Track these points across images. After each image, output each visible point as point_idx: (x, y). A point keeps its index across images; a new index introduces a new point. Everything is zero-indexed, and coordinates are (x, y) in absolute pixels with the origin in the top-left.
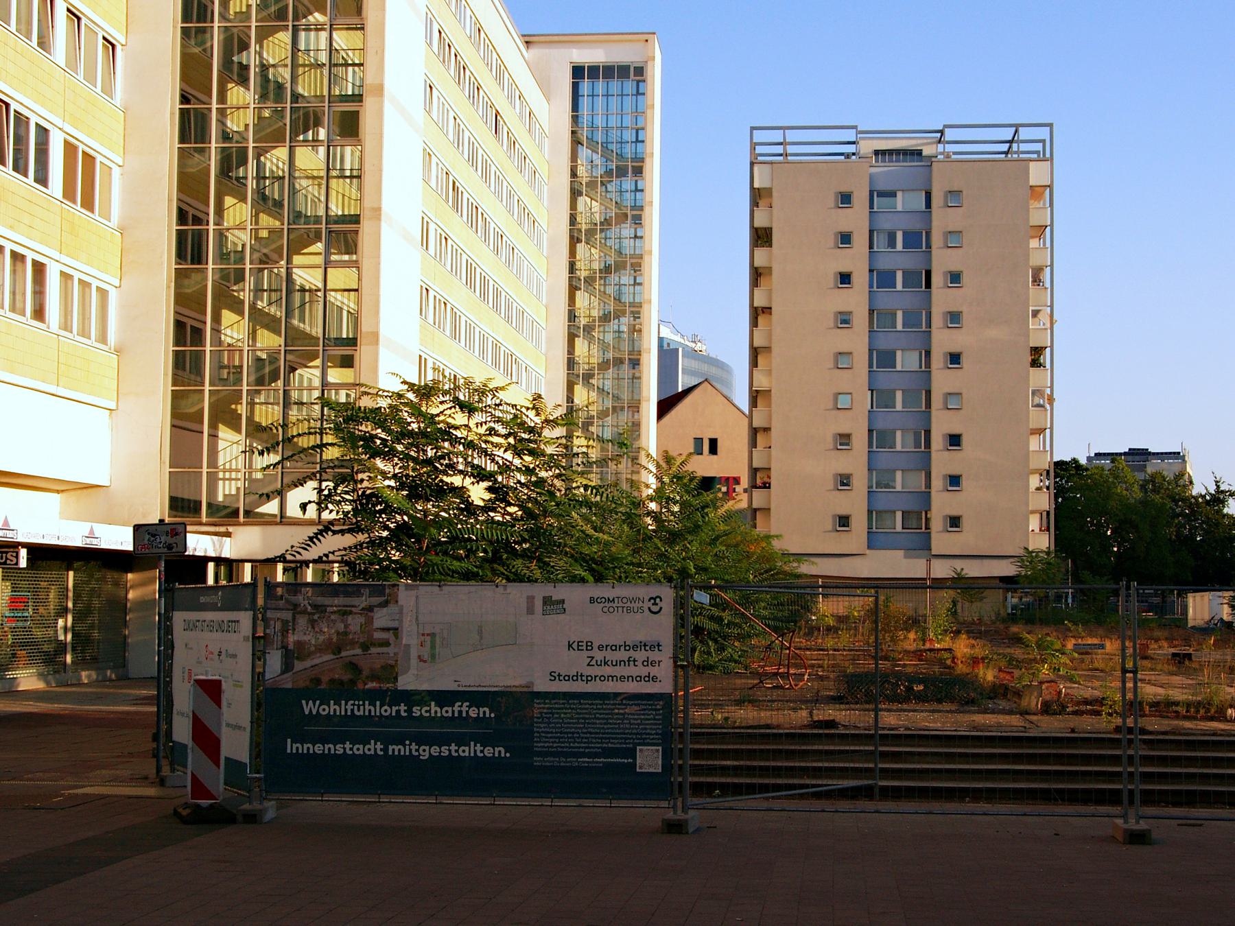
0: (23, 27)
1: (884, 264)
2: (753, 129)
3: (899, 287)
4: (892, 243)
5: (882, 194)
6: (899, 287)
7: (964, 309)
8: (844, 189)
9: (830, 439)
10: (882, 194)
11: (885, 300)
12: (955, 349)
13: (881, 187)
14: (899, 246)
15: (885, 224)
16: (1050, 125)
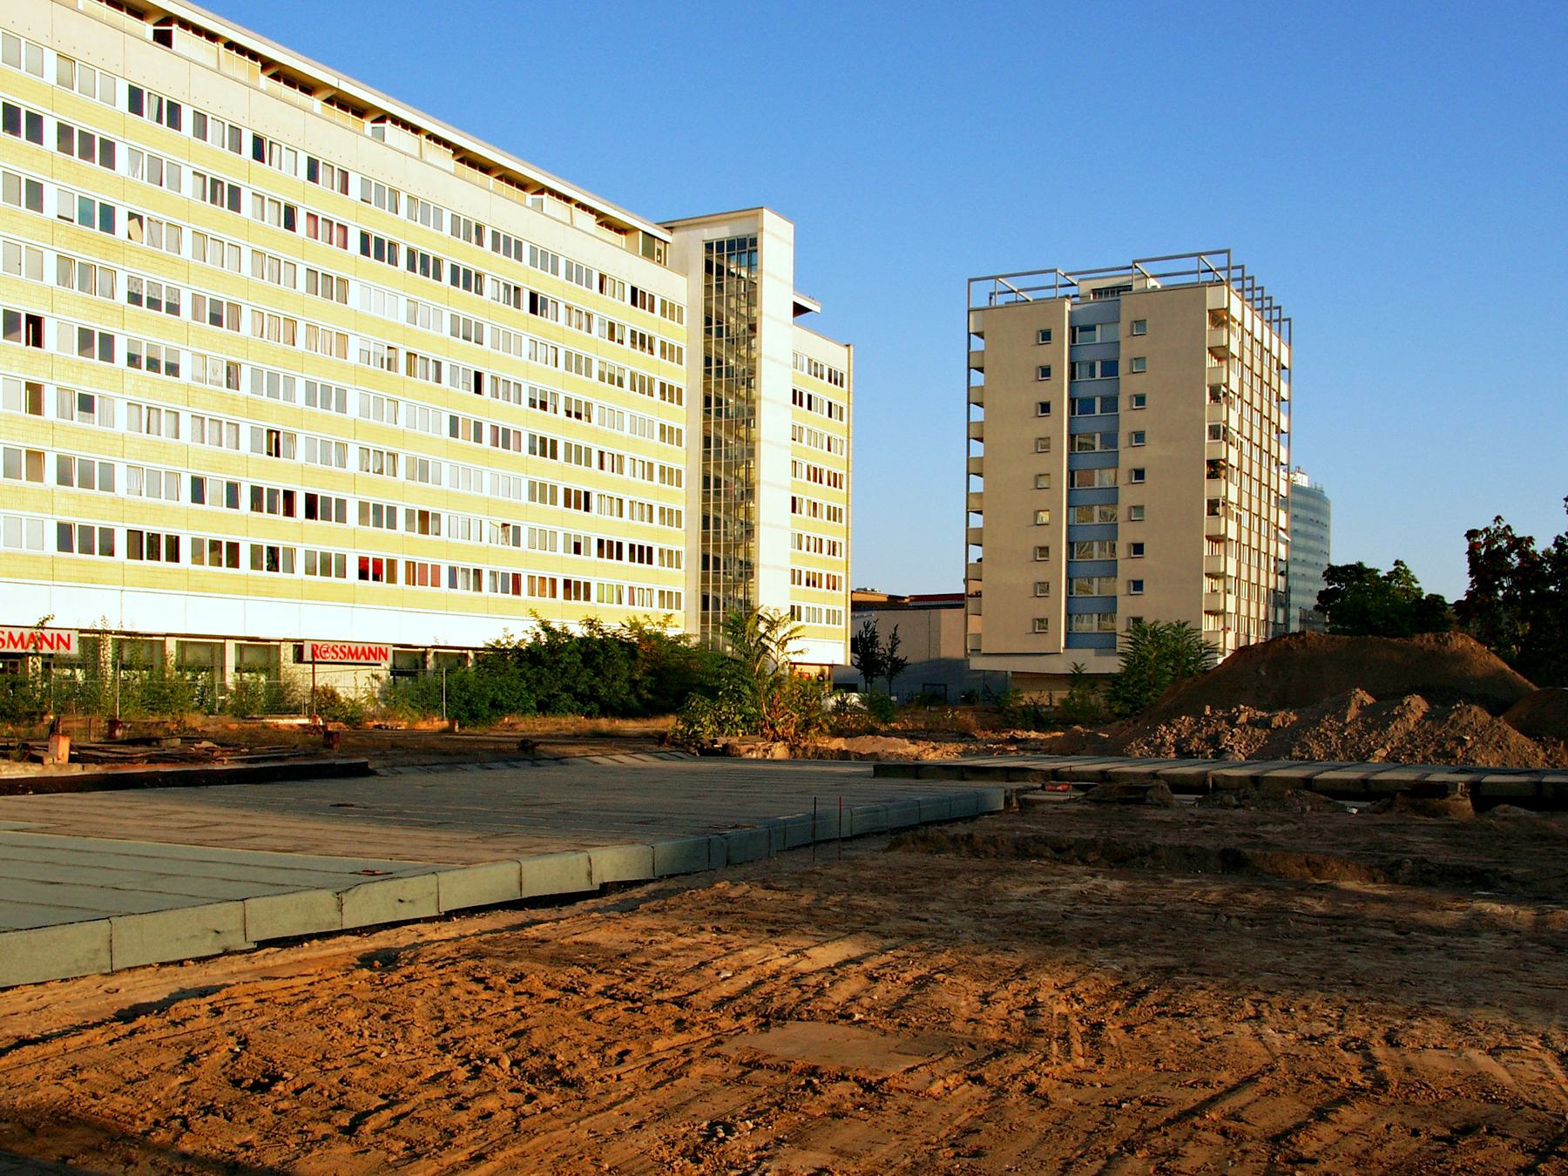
0: (174, 244)
1: (1083, 392)
2: (970, 280)
3: (1098, 412)
4: (1092, 374)
5: (1084, 329)
6: (1098, 412)
7: (1147, 429)
8: (1045, 327)
9: (1031, 551)
10: (1084, 329)
11: (1085, 423)
12: (1139, 466)
13: (1081, 322)
14: (1098, 375)
15: (1084, 355)
16: (1228, 251)
